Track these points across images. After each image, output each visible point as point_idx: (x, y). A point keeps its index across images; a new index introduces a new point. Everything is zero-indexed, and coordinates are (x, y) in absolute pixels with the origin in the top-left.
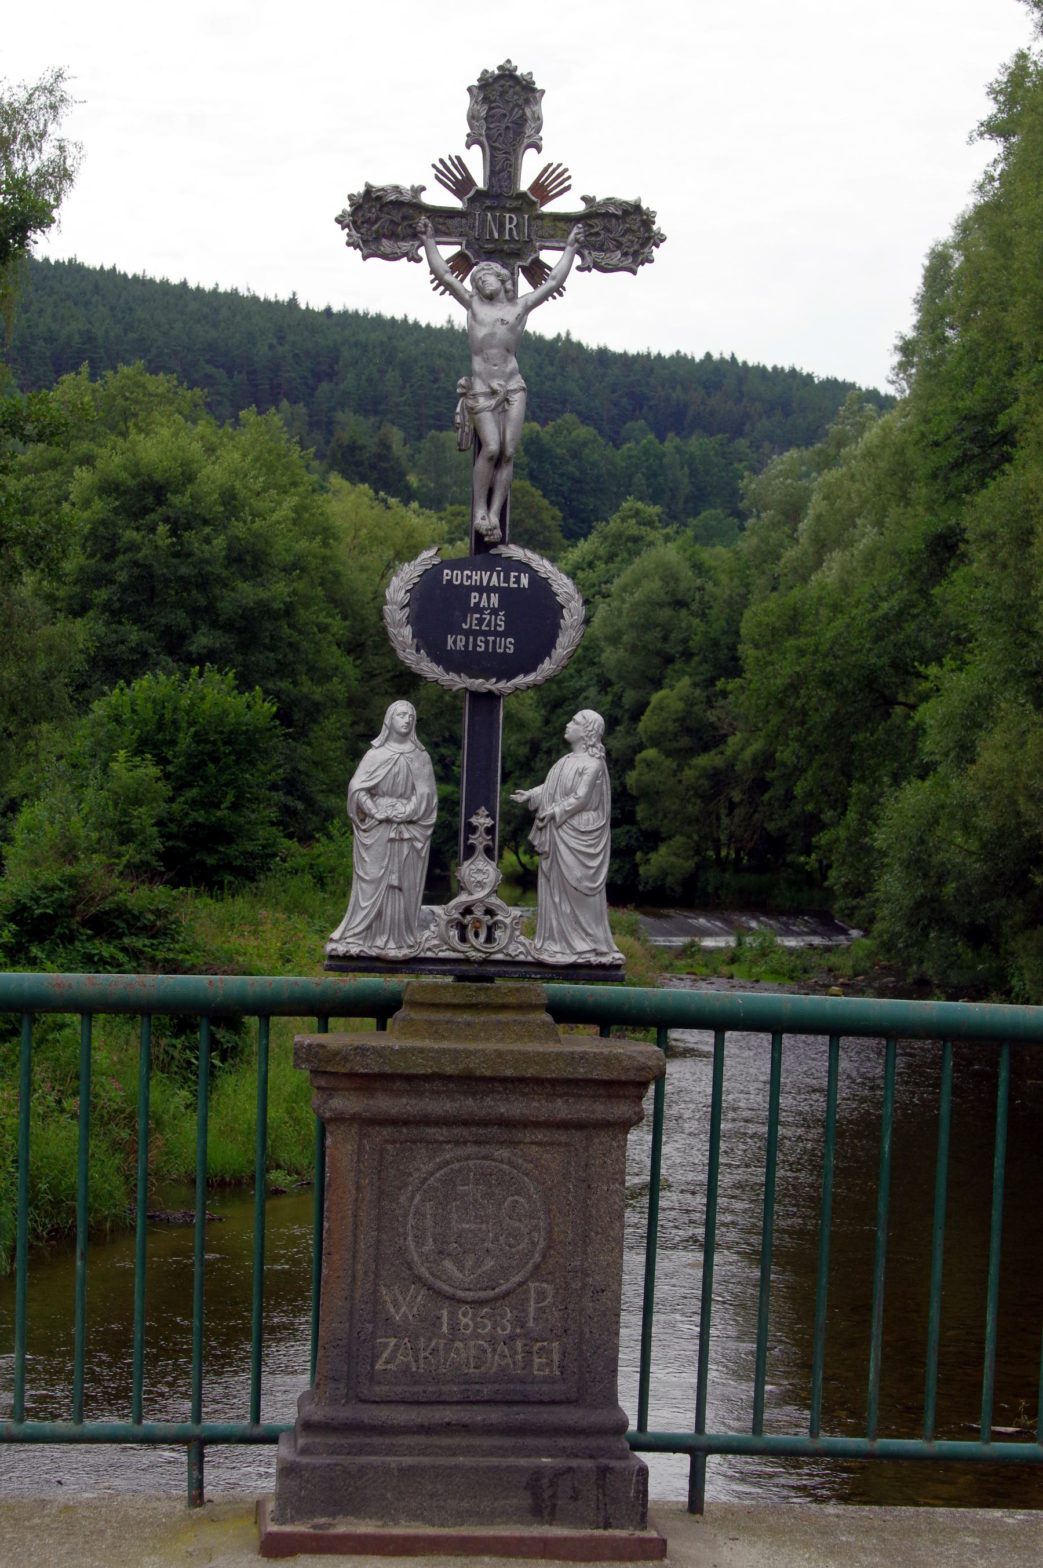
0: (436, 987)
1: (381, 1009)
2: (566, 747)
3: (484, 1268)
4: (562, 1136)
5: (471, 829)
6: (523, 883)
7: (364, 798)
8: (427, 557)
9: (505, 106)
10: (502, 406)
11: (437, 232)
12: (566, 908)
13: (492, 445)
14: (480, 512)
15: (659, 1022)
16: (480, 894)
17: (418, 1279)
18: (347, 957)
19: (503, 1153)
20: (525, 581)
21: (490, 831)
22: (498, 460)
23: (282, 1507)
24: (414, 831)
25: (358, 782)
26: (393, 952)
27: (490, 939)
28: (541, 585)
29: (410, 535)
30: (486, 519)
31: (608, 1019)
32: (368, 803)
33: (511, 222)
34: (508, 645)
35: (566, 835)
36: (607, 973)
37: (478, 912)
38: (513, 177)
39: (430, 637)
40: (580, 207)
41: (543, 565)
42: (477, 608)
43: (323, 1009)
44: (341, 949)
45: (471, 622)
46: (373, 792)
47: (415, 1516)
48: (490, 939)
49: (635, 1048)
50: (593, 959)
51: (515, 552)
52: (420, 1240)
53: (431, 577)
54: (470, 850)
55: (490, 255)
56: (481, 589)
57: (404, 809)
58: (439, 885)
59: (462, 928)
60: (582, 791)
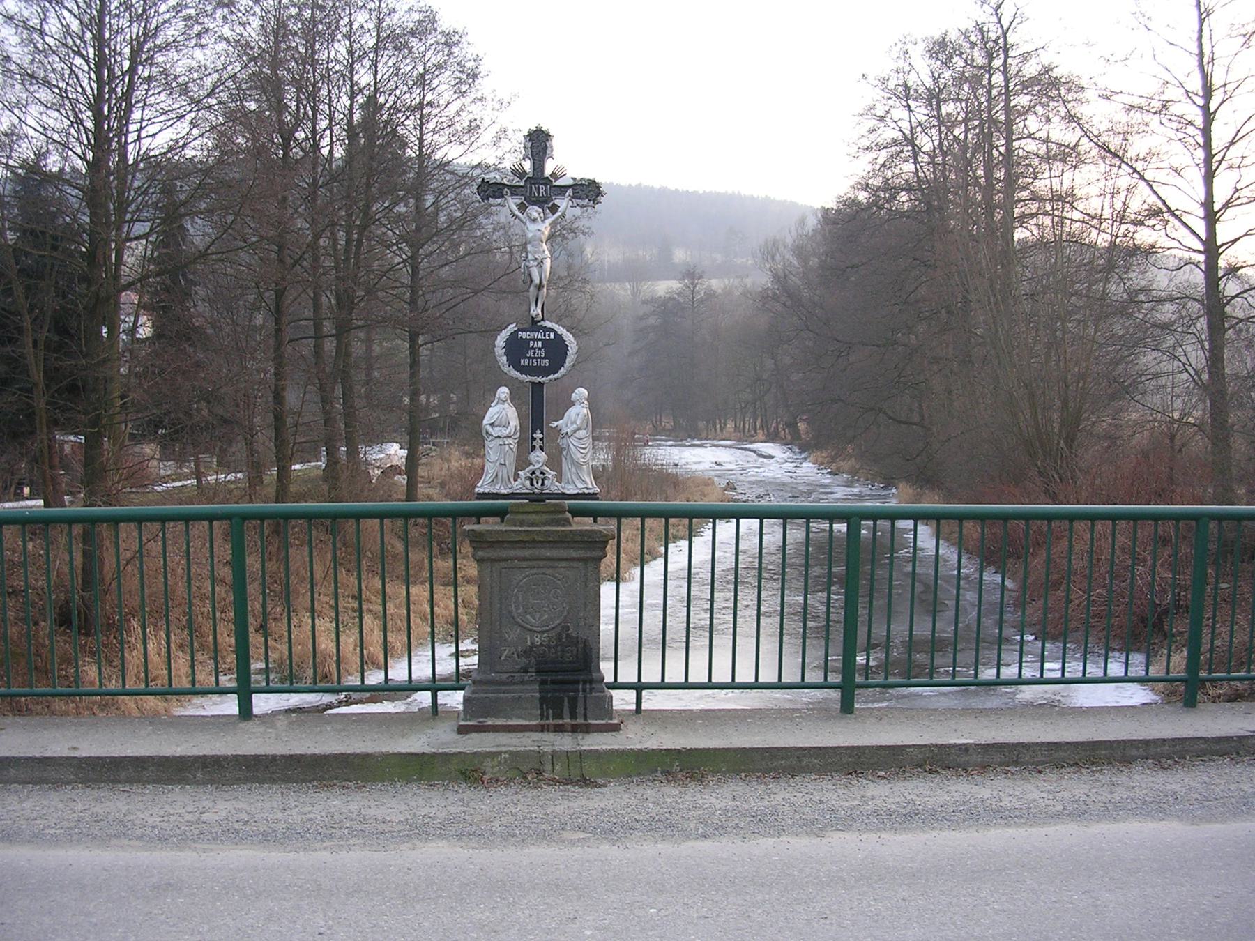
0: (522, 505)
1: (501, 513)
2: (573, 404)
3: (91, 56)
4: (575, 564)
5: (534, 439)
6: (555, 462)
7: (489, 428)
8: (512, 327)
9: (538, 142)
10: (540, 264)
11: (512, 194)
12: (574, 470)
13: (537, 281)
14: (533, 308)
15: (619, 514)
16: (538, 466)
17: (517, 623)
18: (484, 494)
19: (548, 571)
20: (552, 336)
21: (542, 439)
22: (540, 287)
23: (465, 715)
24: (510, 441)
25: (485, 422)
26: (503, 491)
27: (543, 484)
28: (559, 337)
29: (462, 478)
30: (536, 311)
31: (595, 514)
32: (490, 430)
33: (542, 188)
34: (546, 363)
35: (572, 440)
36: (592, 496)
37: (538, 473)
38: (543, 171)
39: (514, 363)
40: (571, 182)
41: (560, 330)
42: (533, 348)
43: (478, 514)
44: (481, 490)
45: (530, 354)
46: (492, 425)
47: (520, 717)
48: (543, 484)
49: (606, 526)
50: (586, 491)
51: (548, 324)
52: (517, 608)
53: (514, 334)
54: (533, 448)
55: (534, 203)
56: (534, 340)
57: (505, 432)
58: (522, 462)
59: (531, 480)
60: (578, 422)
